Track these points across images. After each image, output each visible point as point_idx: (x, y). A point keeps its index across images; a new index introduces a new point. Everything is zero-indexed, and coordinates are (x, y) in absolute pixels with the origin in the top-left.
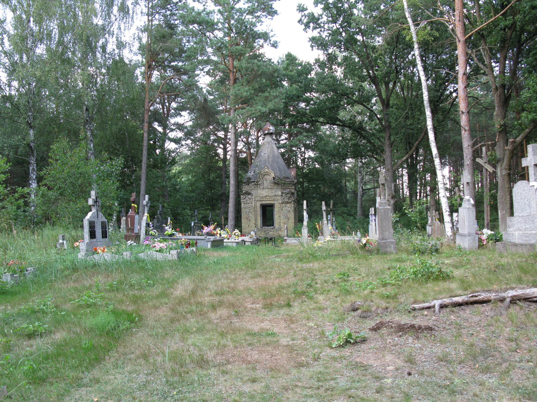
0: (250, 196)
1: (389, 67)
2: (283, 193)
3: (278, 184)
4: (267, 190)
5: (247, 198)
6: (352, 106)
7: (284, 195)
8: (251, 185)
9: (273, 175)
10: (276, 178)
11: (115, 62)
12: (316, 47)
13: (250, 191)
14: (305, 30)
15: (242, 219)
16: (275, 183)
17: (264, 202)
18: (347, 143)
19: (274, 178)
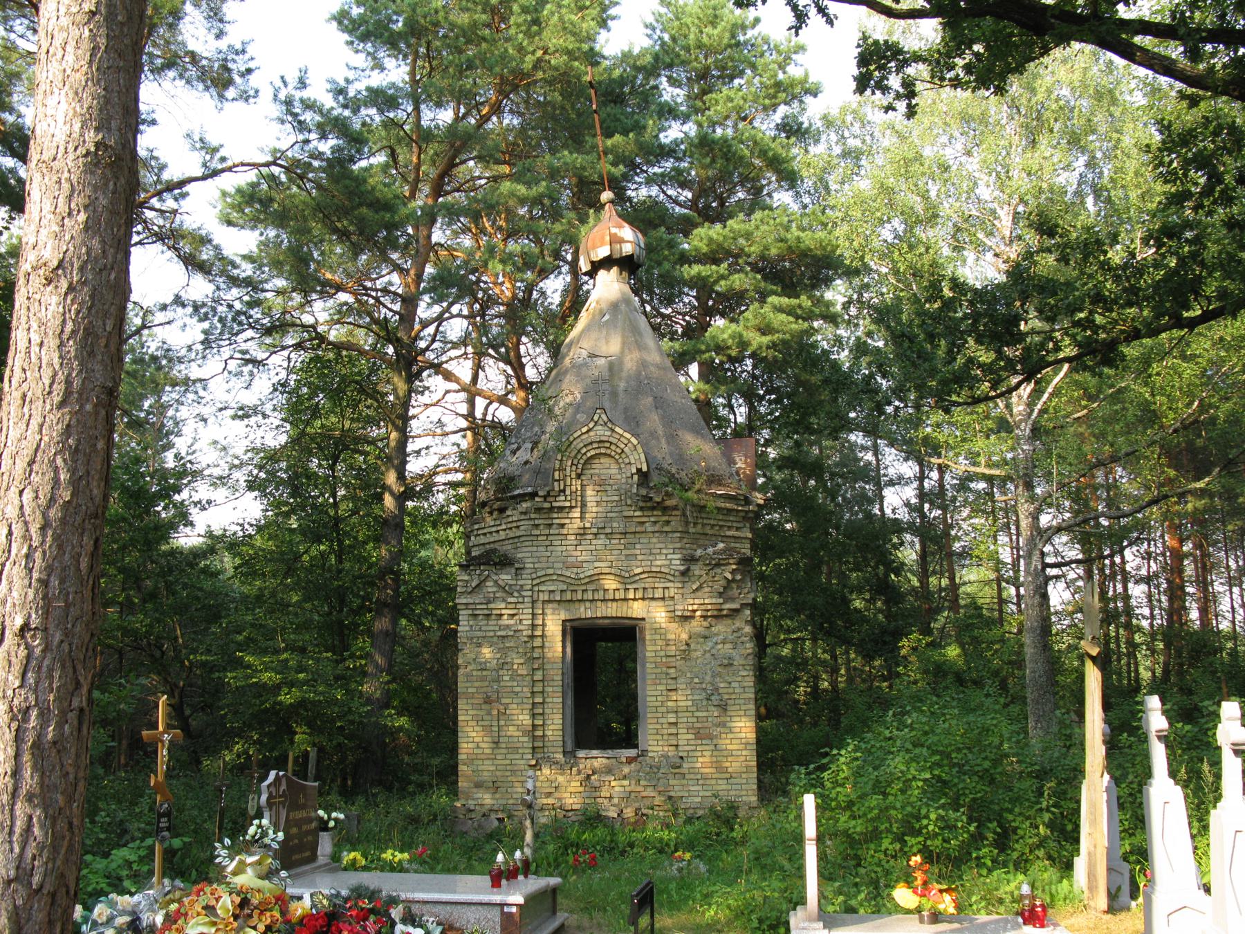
0: (506, 577)
1: (144, 601)
2: (690, 560)
3: (665, 510)
4: (602, 540)
5: (490, 586)
6: (106, 855)
7: (697, 570)
8: (513, 514)
9: (638, 460)
10: (655, 479)
11: (399, 104)
12: (295, 153)
13: (507, 548)
14: (331, 81)
15: (462, 704)
16: (648, 505)
17: (585, 612)
18: (839, 485)
19: (644, 476)
